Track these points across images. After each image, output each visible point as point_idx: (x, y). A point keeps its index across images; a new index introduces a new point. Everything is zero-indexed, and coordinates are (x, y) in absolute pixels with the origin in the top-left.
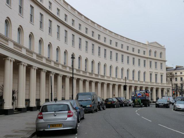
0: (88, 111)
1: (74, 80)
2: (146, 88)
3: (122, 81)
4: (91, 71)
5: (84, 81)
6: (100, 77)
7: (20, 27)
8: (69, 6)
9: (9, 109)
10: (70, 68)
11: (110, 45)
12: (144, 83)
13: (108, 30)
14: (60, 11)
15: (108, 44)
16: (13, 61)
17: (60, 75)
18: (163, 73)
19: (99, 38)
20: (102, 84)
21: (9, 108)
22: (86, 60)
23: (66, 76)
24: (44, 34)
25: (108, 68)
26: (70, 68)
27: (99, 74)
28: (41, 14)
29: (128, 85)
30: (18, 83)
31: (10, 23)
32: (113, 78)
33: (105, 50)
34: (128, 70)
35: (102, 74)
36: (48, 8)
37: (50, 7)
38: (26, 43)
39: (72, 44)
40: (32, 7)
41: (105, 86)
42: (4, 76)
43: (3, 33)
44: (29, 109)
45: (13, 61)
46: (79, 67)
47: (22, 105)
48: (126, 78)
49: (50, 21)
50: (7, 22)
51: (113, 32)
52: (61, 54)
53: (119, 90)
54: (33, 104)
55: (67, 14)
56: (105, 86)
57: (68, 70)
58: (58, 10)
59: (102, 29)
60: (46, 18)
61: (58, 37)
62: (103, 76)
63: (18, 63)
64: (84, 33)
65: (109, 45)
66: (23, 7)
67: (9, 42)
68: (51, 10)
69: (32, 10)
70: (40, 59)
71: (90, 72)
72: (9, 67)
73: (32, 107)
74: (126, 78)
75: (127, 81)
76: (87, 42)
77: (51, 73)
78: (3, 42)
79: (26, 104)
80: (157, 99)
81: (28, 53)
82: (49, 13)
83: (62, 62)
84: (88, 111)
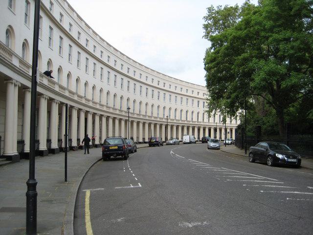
0: (230, 178)
3: (164, 120)
5: (114, 119)
11: (133, 77)
13: (106, 42)
15: (112, 65)
17: (14, 81)
25: (149, 106)
29: (130, 119)
42: (5, 116)
43: (3, 40)
45: (19, 85)
48: (167, 117)
50: (9, 32)
51: (91, 28)
57: (123, 114)
58: (87, 41)
59: (91, 32)
62: (139, 115)
63: (5, 80)
66: (29, 14)
67: (13, 56)
72: (13, 94)
77: (12, 83)
78: (6, 56)
80: (183, 135)
81: (22, 66)
84: (230, 178)
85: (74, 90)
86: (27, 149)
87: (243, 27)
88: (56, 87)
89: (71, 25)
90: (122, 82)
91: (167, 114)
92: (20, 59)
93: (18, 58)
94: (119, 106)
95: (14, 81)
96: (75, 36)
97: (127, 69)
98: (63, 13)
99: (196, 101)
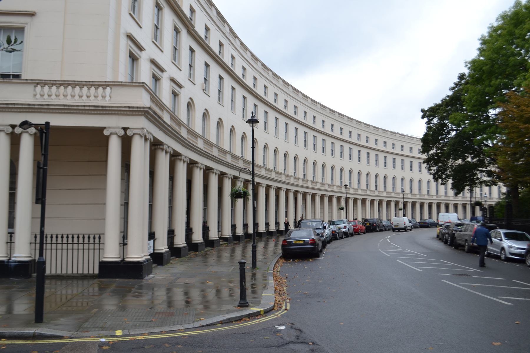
2: (405, 204)
7: (190, 101)
9: (199, 243)
12: (393, 195)
14: (258, 80)
15: (310, 123)
17: (165, 147)
18: (32, 14)
19: (332, 129)
20: (322, 197)
22: (285, 155)
33: (342, 146)
34: (376, 176)
41: (326, 200)
42: (104, 189)
47: (227, 233)
48: (346, 185)
55: (267, 85)
56: (326, 200)
61: (233, 108)
65: (330, 133)
74: (346, 185)
76: (276, 119)
79: (203, 237)
85: (227, 147)
86: (250, 231)
89: (244, 69)
92: (171, 115)
94: (330, 183)
95: (165, 147)
97: (339, 129)
98: (257, 76)
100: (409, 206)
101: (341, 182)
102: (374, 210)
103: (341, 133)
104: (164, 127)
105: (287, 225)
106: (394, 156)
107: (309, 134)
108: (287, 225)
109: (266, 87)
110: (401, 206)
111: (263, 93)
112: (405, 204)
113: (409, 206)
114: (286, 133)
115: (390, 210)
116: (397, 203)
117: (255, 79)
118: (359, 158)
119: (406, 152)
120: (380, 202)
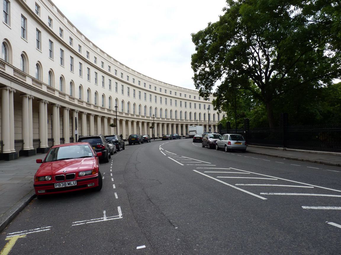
1: (117, 121)
2: (153, 124)
3: (151, 119)
4: (127, 111)
6: (135, 117)
7: (38, 63)
8: (82, 36)
10: (114, 111)
16: (32, 98)
21: (30, 149)
23: (105, 117)
24: (65, 71)
26: (114, 111)
27: (122, 111)
28: (71, 57)
29: (119, 118)
30: (104, 125)
31: (26, 59)
32: (147, 117)
34: (151, 108)
35: (138, 114)
36: (77, 51)
37: (88, 56)
38: (45, 79)
39: (79, 74)
40: (51, 42)
41: (130, 124)
44: (24, 154)
45: (32, 98)
46: (110, 107)
48: (154, 115)
49: (72, 58)
50: (6, 44)
52: (125, 106)
53: (148, 126)
54: (29, 146)
55: (89, 51)
56: (130, 124)
57: (112, 113)
59: (91, 45)
60: (67, 54)
64: (114, 75)
67: (27, 77)
68: (81, 53)
69: (62, 53)
70: (62, 96)
71: (127, 112)
72: (8, 100)
73: (44, 148)
75: (155, 119)
82: (82, 58)
83: (107, 106)
87: (218, 25)
88: (84, 105)
89: (71, 39)
90: (299, 160)
91: (153, 112)
93: (13, 68)
94: (105, 106)
96: (76, 49)
99: (178, 101)
100: (156, 125)
101: (150, 114)
102: (144, 127)
103: (122, 76)
104: (22, 84)
105: (51, 140)
106: (181, 100)
107: (201, 105)
108: (51, 140)
109: (103, 63)
110: (151, 125)
111: (101, 66)
112: (153, 124)
113: (156, 125)
114: (122, 90)
115: (164, 127)
116: (148, 123)
117: (88, 53)
118: (156, 100)
119: (192, 98)
120: (138, 123)
